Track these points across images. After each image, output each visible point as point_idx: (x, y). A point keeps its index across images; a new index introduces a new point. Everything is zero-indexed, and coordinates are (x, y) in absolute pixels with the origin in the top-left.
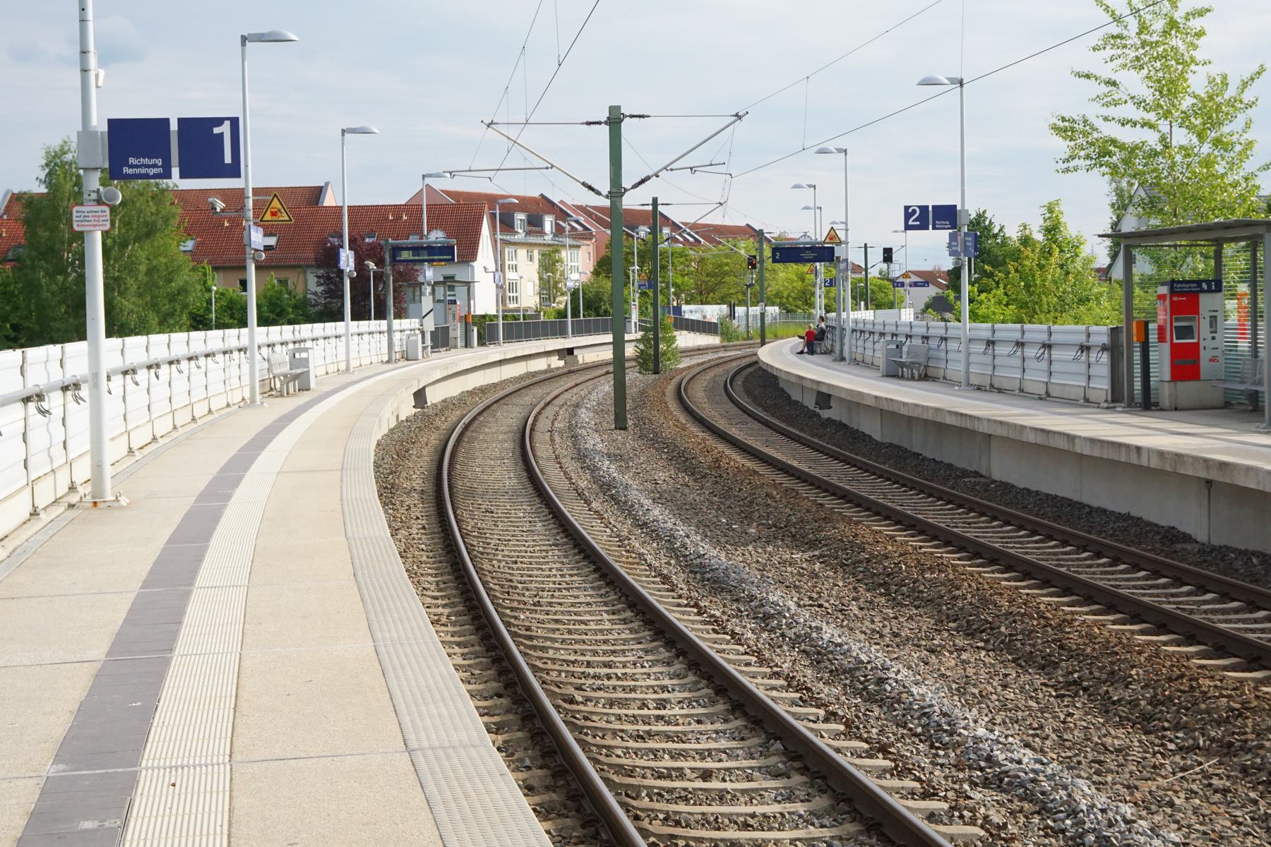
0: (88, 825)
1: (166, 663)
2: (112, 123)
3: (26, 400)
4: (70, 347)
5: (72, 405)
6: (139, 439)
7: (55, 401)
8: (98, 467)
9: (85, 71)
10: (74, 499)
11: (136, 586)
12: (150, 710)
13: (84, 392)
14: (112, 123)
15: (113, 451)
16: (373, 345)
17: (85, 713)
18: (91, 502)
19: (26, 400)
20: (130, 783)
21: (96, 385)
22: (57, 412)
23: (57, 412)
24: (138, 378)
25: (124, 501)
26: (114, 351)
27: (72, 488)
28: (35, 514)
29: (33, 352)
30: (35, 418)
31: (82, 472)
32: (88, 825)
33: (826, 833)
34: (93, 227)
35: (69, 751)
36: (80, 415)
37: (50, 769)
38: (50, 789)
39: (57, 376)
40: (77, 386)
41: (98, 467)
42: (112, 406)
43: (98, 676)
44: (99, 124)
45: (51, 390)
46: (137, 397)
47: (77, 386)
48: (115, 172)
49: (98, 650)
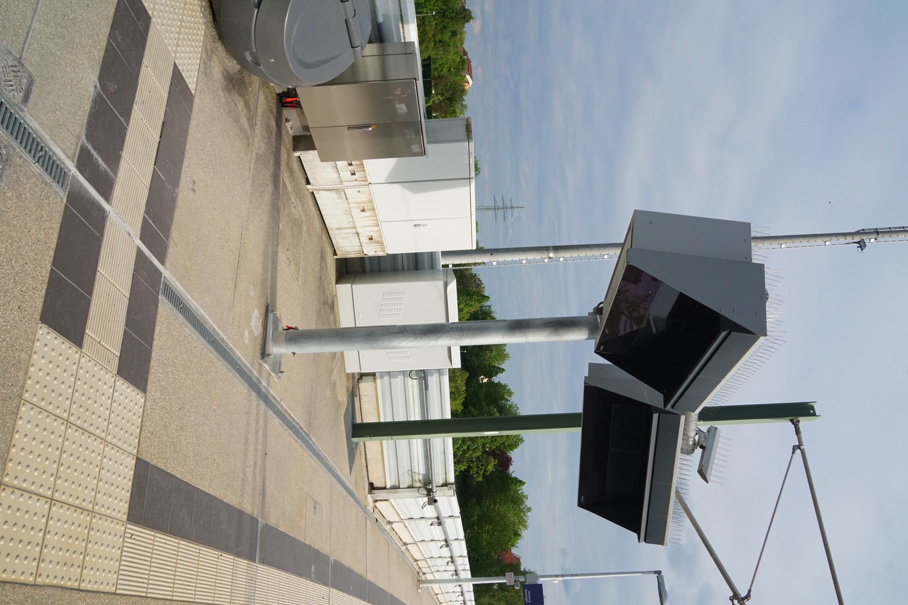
0: (313, 568)
1: (365, 600)
2: (541, 585)
3: (451, 557)
4: (469, 572)
5: (450, 573)
6: (440, 597)
7: (451, 567)
8: (431, 582)
9: (557, 576)
10: (421, 574)
11: (391, 592)
12: (349, 593)
13: (455, 577)
14: (541, 585)
15: (436, 587)
16: (440, 562)
17: (349, 571)
18: (419, 579)
19: (451, 557)
20: (325, 584)
21: (457, 581)
22: (448, 568)
23: (448, 568)
24: (444, 548)
25: (420, 591)
26: (469, 587)
27: (424, 574)
28: (416, 560)
29: (467, 559)
30: (440, 544)
31: (429, 577)
32: (313, 568)
33: (247, 342)
34: (505, 580)
35: (337, 565)
36: (447, 576)
37: (332, 558)
38: (326, 558)
39: (460, 568)
40: (457, 575)
41: (431, 582)
42: (451, 587)
43: (361, 576)
44: (540, 581)
45: (455, 566)
46: (454, 597)
47: (457, 575)
48: (524, 586)
49: (370, 577)
